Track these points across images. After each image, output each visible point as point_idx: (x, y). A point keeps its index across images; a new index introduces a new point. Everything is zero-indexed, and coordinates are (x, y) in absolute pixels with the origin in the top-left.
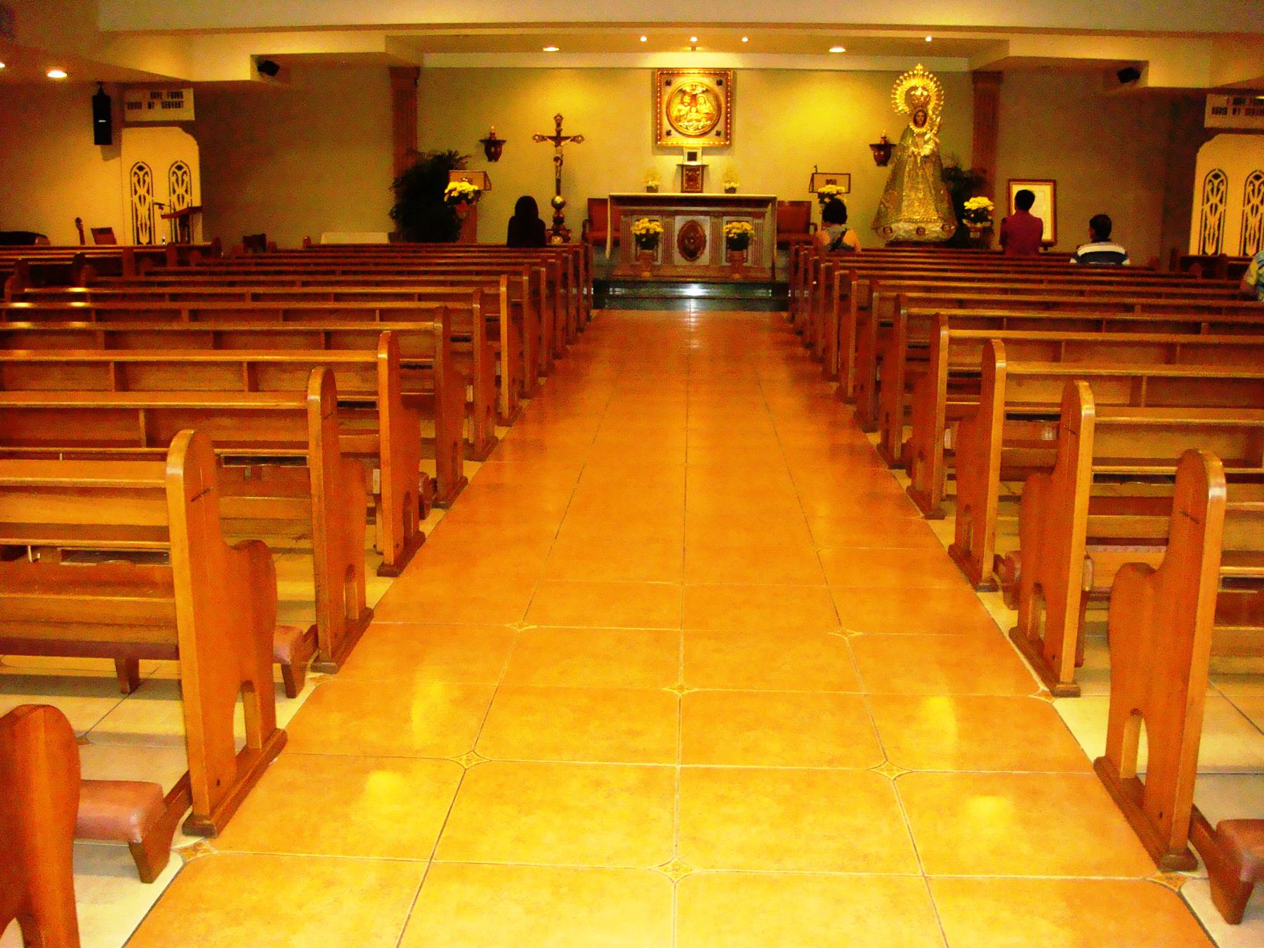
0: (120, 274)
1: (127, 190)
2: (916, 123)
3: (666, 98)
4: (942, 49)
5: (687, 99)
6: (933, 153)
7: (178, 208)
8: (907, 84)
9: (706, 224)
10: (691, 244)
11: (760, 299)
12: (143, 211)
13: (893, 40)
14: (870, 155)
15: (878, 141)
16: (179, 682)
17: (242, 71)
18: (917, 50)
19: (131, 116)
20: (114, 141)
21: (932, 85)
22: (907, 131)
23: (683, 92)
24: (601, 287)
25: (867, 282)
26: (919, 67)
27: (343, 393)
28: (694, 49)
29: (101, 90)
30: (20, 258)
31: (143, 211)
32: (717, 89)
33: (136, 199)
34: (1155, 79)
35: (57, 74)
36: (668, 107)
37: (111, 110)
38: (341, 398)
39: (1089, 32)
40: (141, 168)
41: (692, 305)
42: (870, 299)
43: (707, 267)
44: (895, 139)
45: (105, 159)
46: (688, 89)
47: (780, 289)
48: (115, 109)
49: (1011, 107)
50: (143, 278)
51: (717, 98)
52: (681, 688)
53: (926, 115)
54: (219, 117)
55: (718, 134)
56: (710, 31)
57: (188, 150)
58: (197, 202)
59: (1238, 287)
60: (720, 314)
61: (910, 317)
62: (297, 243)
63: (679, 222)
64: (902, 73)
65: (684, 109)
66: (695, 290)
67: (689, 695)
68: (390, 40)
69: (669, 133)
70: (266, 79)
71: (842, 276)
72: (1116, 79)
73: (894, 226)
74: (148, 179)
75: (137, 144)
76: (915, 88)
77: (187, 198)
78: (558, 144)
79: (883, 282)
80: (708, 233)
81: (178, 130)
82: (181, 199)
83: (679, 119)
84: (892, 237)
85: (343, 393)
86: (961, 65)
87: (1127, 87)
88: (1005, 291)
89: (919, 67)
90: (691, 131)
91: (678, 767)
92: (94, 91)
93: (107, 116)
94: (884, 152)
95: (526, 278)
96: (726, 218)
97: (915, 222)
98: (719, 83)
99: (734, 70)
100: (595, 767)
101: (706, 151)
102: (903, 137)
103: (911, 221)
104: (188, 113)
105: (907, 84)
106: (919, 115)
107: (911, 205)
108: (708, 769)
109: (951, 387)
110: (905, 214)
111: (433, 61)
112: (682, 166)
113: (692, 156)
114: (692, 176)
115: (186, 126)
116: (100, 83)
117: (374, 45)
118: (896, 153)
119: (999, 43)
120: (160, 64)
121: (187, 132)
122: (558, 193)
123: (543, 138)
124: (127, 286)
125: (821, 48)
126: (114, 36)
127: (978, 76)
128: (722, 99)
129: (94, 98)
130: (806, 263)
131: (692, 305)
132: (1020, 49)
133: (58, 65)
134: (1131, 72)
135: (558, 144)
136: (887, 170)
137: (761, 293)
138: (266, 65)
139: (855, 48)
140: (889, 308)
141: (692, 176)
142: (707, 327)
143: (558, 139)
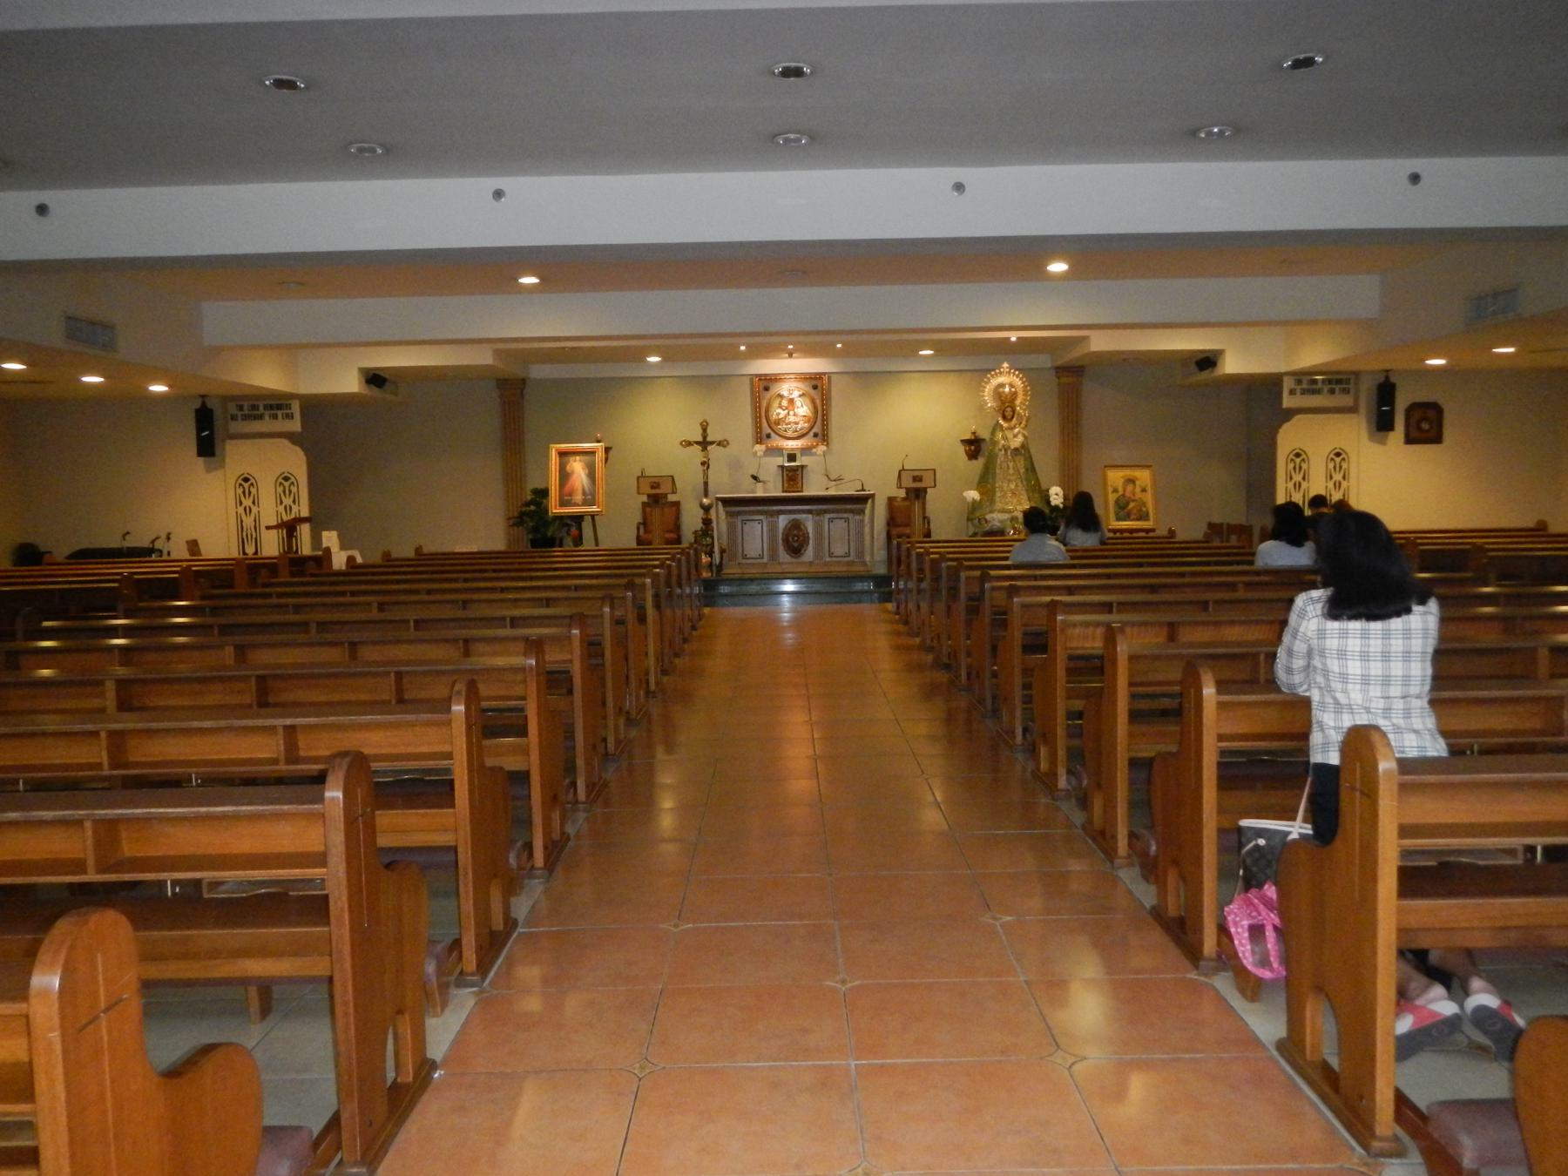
0: (232, 587)
1: (232, 502)
2: (1004, 418)
3: (764, 404)
4: (1026, 346)
5: (785, 403)
6: (1023, 446)
7: (285, 518)
8: (1001, 379)
9: (809, 523)
10: (795, 542)
11: (863, 592)
12: (248, 522)
13: (990, 340)
14: (961, 450)
15: (968, 436)
16: (331, 980)
17: (349, 383)
18: (1002, 349)
19: (238, 427)
20: (217, 452)
21: (1018, 382)
22: (997, 426)
23: (781, 396)
24: (710, 586)
25: (977, 573)
26: (1006, 365)
27: (489, 699)
28: (791, 355)
29: (204, 404)
30: (126, 571)
31: (248, 522)
32: (812, 392)
33: (241, 510)
34: (1232, 365)
35: (158, 388)
36: (767, 411)
37: (211, 425)
38: (484, 704)
39: (1155, 326)
40: (246, 480)
41: (785, 599)
42: (982, 591)
43: (811, 563)
44: (985, 434)
45: (208, 471)
46: (785, 393)
47: (882, 581)
48: (218, 423)
49: (1095, 398)
50: (258, 590)
51: (813, 402)
52: (844, 982)
53: (1014, 411)
54: (322, 426)
55: (816, 435)
56: (802, 338)
57: (295, 462)
58: (305, 513)
59: (1251, 563)
60: (808, 608)
61: (1024, 606)
62: (409, 553)
63: (783, 521)
64: (989, 371)
65: (783, 413)
66: (789, 586)
67: (851, 989)
68: (497, 353)
69: (768, 436)
70: (375, 392)
71: (949, 567)
72: (1193, 367)
73: (988, 517)
74: (253, 490)
75: (240, 456)
76: (1002, 385)
77: (295, 509)
78: (704, 449)
79: (993, 573)
80: (810, 529)
81: (286, 442)
82: (288, 509)
83: (778, 422)
84: (987, 527)
85: (489, 699)
86: (1045, 361)
87: (1205, 375)
88: (1108, 576)
89: (1006, 365)
90: (790, 434)
91: (853, 1064)
92: (198, 404)
93: (211, 429)
94: (974, 446)
95: (648, 581)
96: (828, 516)
97: (1009, 511)
98: (815, 387)
99: (829, 374)
100: (770, 1068)
101: (806, 451)
102: (993, 433)
103: (1003, 511)
104: (295, 425)
105: (1001, 379)
106: (1006, 407)
107: (1004, 496)
108: (882, 1066)
109: (1070, 672)
110: (999, 505)
111: (538, 372)
112: (782, 467)
113: (792, 457)
114: (793, 475)
115: (290, 436)
116: (203, 396)
117: (482, 358)
118: (985, 448)
119: (1085, 338)
120: (266, 377)
121: (294, 443)
122: (706, 495)
123: (689, 444)
124: (248, 597)
125: (908, 349)
126: (218, 351)
127: (1061, 370)
128: (818, 402)
129: (197, 411)
130: (909, 555)
131: (785, 599)
132: (1100, 343)
133: (156, 381)
134: (1207, 361)
135: (704, 449)
136: (979, 463)
137: (859, 586)
138: (375, 379)
139: (942, 349)
140: (1000, 597)
141: (793, 475)
142: (798, 623)
143: (704, 444)
